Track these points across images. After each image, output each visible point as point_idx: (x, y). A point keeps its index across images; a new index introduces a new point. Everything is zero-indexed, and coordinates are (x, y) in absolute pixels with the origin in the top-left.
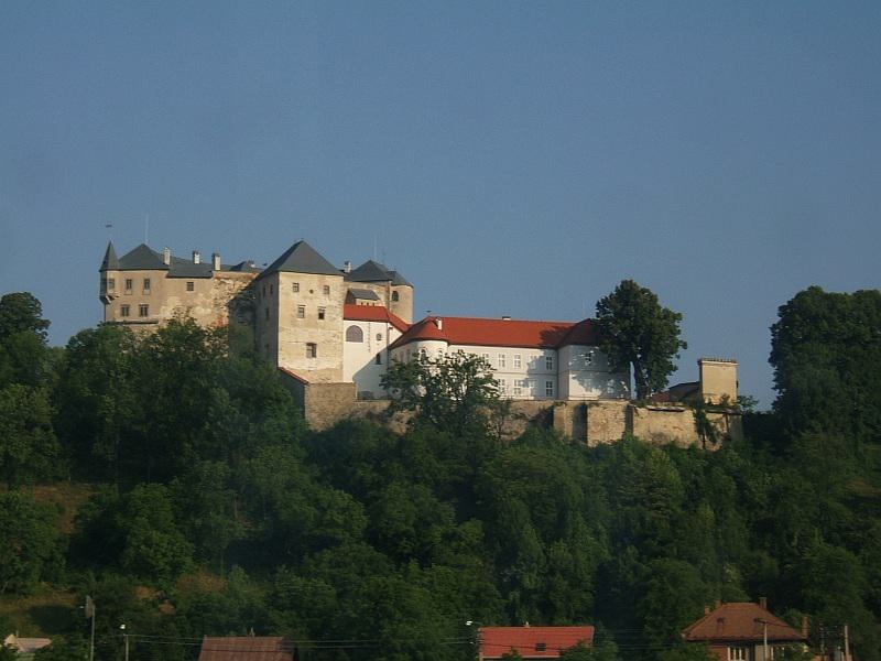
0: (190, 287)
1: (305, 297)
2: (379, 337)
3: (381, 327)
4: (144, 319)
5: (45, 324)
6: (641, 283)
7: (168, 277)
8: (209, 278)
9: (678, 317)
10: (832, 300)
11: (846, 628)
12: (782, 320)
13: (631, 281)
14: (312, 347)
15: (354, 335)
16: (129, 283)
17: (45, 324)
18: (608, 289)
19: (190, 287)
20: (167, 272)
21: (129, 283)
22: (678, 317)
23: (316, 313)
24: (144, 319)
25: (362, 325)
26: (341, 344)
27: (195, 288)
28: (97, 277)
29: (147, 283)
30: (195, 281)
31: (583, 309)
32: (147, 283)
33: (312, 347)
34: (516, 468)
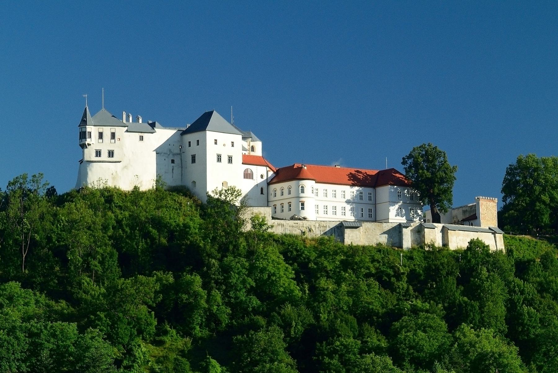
0: (141, 138)
4: (98, 159)
7: (127, 131)
8: (152, 133)
13: (519, 161)
16: (101, 135)
19: (141, 138)
20: (126, 128)
21: (101, 135)
24: (98, 159)
25: (253, 168)
28: (78, 131)
29: (113, 135)
30: (145, 135)
31: (393, 161)
32: (113, 135)
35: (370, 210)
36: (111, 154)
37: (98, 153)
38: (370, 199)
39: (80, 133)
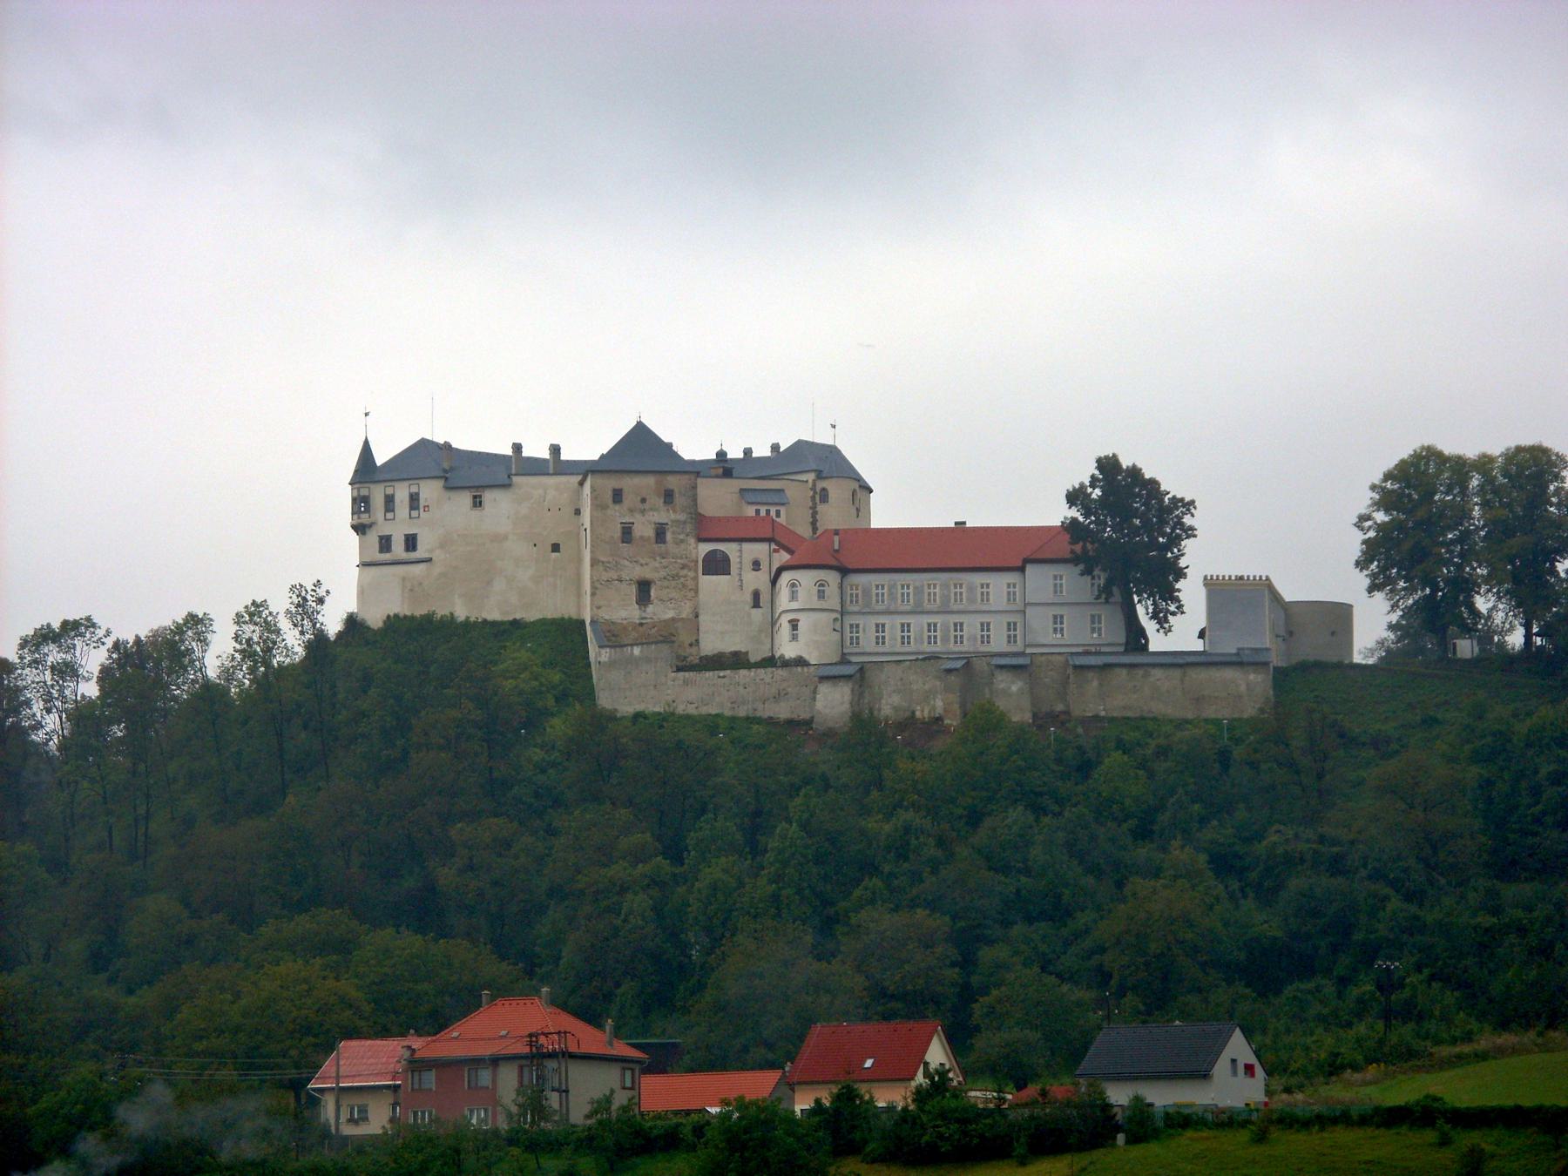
2: (756, 565)
3: (760, 550)
4: (986, 618)
5: (1373, 488)
9: (1189, 505)
12: (1071, 527)
14: (644, 587)
15: (716, 564)
16: (389, 501)
17: (1373, 488)
18: (1083, 472)
22: (1189, 505)
23: (650, 532)
25: (730, 549)
26: (696, 578)
27: (610, 493)
29: (414, 500)
32: (414, 500)
33: (644, 587)
34: (245, 722)
35: (1011, 626)
36: (411, 542)
38: (1011, 597)
39: (354, 500)
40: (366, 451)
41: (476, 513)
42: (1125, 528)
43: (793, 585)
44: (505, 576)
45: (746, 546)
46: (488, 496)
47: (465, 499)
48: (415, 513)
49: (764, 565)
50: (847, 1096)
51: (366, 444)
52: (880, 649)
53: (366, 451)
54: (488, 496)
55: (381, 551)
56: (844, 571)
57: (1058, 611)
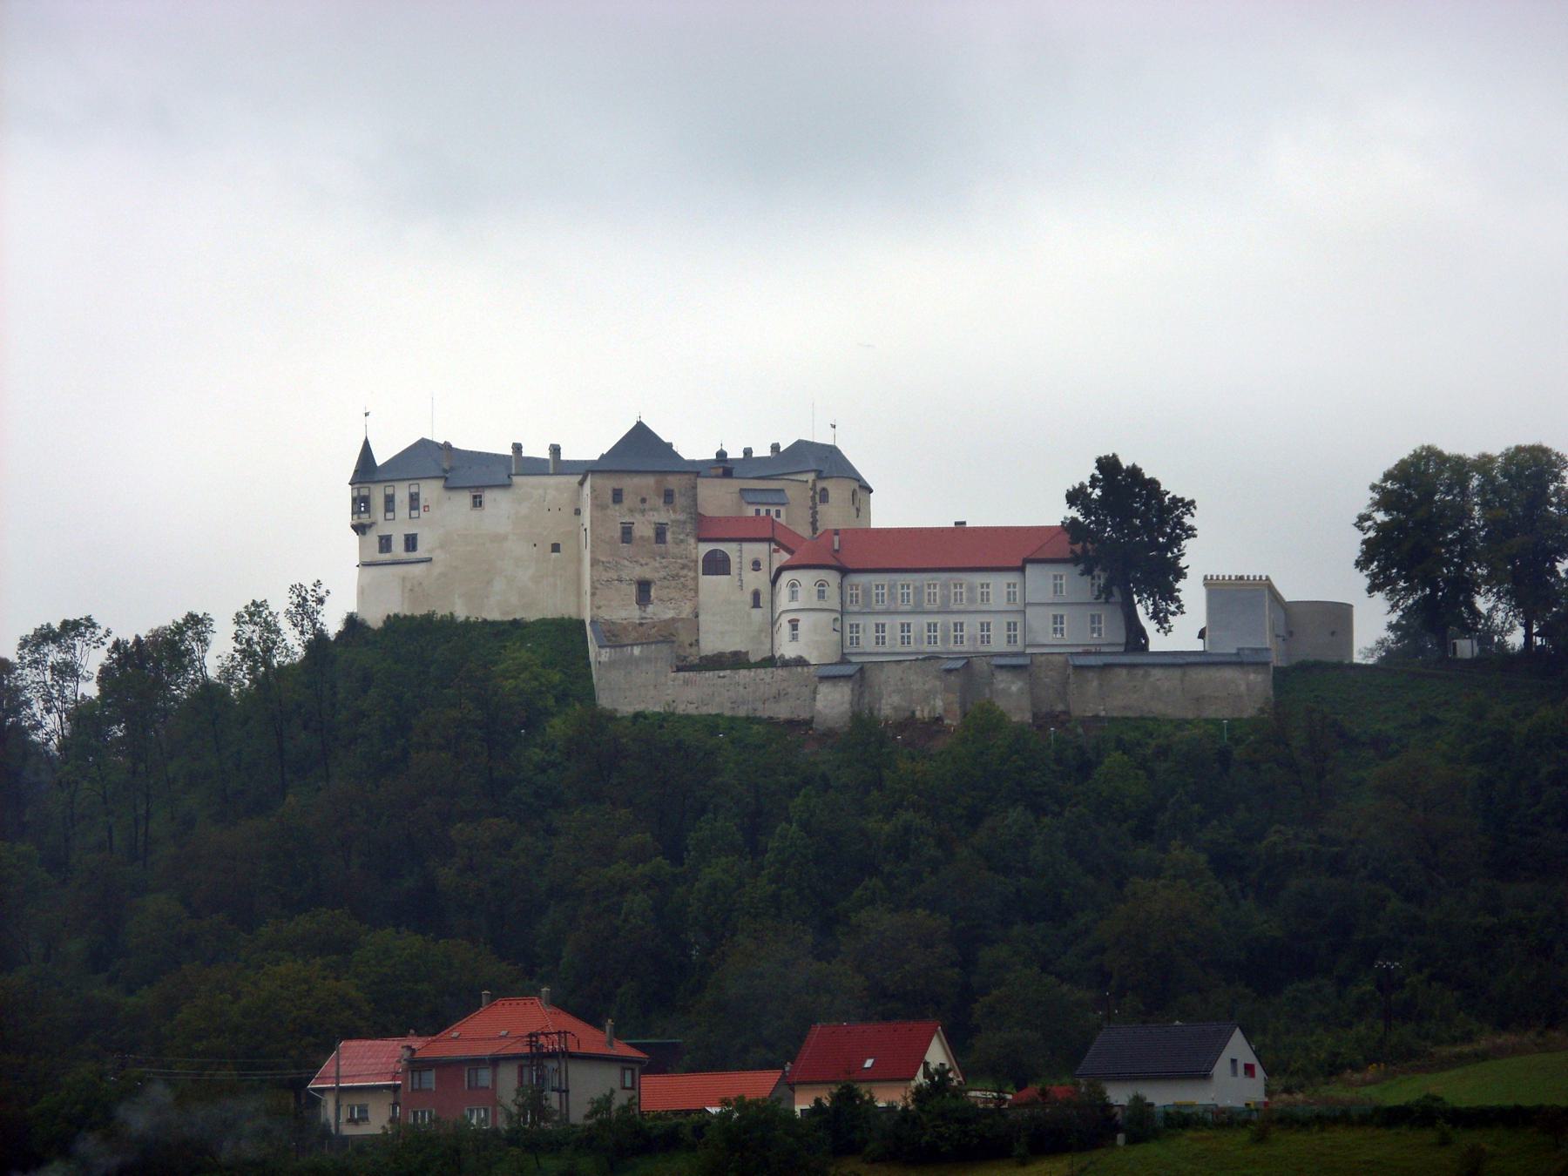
1: (631, 511)
2: (756, 565)
4: (986, 618)
5: (1373, 488)
6: (1478, 432)
9: (1189, 505)
10: (1459, 467)
11: (973, 1094)
12: (1071, 526)
14: (644, 587)
15: (716, 564)
16: (389, 501)
17: (1373, 488)
18: (1084, 472)
22: (1189, 505)
23: (650, 532)
25: (730, 549)
26: (696, 579)
29: (414, 500)
32: (414, 500)
33: (644, 587)
36: (411, 542)
37: (385, 543)
39: (354, 500)
40: (366, 452)
41: (476, 513)
42: (1127, 527)
43: (793, 585)
44: (503, 573)
45: (746, 546)
46: (488, 496)
47: (465, 498)
48: (415, 513)
49: (764, 565)
50: (847, 1096)
51: (366, 443)
52: (881, 649)
53: (366, 452)
54: (488, 496)
55: (381, 551)
56: (844, 571)
57: (1059, 611)
